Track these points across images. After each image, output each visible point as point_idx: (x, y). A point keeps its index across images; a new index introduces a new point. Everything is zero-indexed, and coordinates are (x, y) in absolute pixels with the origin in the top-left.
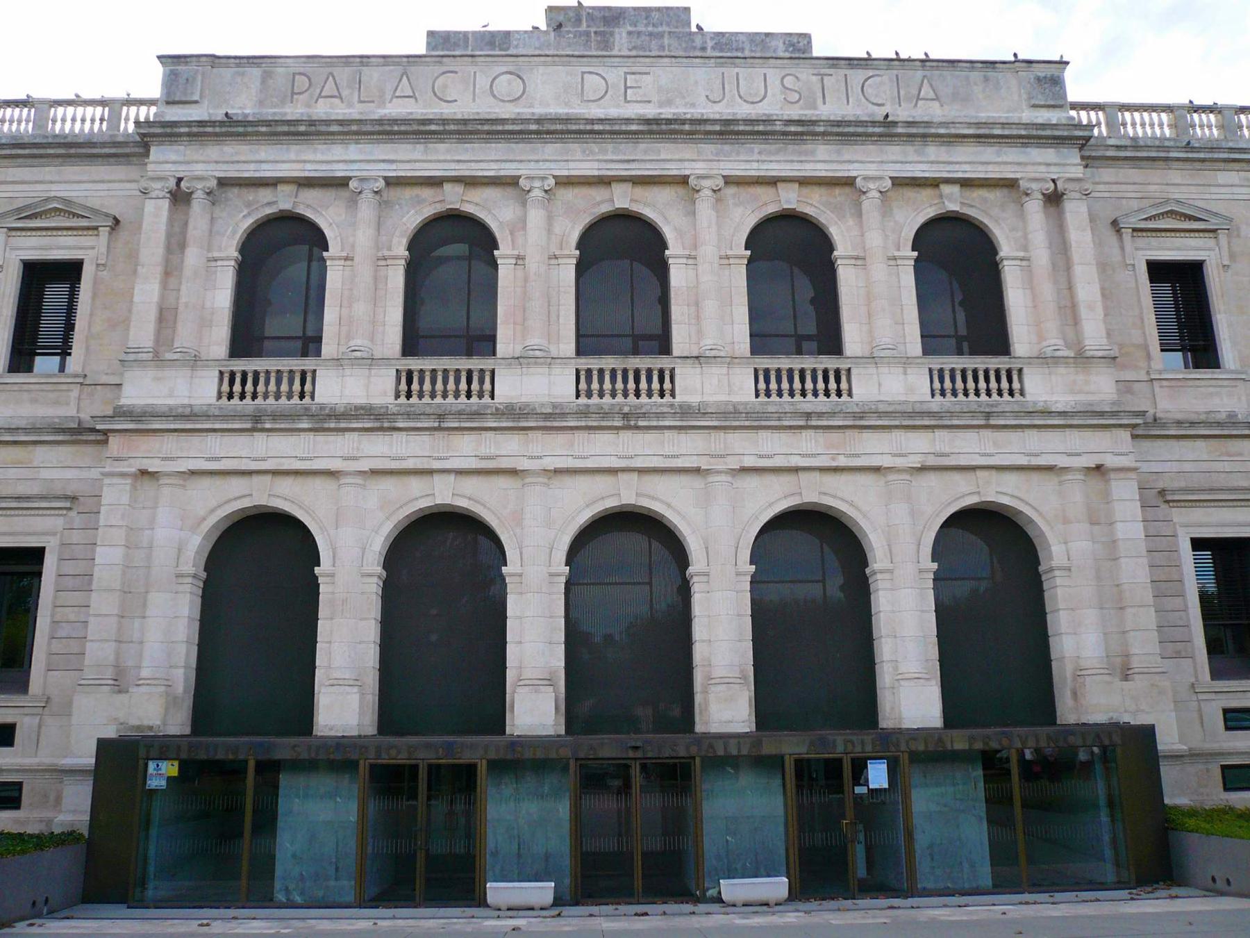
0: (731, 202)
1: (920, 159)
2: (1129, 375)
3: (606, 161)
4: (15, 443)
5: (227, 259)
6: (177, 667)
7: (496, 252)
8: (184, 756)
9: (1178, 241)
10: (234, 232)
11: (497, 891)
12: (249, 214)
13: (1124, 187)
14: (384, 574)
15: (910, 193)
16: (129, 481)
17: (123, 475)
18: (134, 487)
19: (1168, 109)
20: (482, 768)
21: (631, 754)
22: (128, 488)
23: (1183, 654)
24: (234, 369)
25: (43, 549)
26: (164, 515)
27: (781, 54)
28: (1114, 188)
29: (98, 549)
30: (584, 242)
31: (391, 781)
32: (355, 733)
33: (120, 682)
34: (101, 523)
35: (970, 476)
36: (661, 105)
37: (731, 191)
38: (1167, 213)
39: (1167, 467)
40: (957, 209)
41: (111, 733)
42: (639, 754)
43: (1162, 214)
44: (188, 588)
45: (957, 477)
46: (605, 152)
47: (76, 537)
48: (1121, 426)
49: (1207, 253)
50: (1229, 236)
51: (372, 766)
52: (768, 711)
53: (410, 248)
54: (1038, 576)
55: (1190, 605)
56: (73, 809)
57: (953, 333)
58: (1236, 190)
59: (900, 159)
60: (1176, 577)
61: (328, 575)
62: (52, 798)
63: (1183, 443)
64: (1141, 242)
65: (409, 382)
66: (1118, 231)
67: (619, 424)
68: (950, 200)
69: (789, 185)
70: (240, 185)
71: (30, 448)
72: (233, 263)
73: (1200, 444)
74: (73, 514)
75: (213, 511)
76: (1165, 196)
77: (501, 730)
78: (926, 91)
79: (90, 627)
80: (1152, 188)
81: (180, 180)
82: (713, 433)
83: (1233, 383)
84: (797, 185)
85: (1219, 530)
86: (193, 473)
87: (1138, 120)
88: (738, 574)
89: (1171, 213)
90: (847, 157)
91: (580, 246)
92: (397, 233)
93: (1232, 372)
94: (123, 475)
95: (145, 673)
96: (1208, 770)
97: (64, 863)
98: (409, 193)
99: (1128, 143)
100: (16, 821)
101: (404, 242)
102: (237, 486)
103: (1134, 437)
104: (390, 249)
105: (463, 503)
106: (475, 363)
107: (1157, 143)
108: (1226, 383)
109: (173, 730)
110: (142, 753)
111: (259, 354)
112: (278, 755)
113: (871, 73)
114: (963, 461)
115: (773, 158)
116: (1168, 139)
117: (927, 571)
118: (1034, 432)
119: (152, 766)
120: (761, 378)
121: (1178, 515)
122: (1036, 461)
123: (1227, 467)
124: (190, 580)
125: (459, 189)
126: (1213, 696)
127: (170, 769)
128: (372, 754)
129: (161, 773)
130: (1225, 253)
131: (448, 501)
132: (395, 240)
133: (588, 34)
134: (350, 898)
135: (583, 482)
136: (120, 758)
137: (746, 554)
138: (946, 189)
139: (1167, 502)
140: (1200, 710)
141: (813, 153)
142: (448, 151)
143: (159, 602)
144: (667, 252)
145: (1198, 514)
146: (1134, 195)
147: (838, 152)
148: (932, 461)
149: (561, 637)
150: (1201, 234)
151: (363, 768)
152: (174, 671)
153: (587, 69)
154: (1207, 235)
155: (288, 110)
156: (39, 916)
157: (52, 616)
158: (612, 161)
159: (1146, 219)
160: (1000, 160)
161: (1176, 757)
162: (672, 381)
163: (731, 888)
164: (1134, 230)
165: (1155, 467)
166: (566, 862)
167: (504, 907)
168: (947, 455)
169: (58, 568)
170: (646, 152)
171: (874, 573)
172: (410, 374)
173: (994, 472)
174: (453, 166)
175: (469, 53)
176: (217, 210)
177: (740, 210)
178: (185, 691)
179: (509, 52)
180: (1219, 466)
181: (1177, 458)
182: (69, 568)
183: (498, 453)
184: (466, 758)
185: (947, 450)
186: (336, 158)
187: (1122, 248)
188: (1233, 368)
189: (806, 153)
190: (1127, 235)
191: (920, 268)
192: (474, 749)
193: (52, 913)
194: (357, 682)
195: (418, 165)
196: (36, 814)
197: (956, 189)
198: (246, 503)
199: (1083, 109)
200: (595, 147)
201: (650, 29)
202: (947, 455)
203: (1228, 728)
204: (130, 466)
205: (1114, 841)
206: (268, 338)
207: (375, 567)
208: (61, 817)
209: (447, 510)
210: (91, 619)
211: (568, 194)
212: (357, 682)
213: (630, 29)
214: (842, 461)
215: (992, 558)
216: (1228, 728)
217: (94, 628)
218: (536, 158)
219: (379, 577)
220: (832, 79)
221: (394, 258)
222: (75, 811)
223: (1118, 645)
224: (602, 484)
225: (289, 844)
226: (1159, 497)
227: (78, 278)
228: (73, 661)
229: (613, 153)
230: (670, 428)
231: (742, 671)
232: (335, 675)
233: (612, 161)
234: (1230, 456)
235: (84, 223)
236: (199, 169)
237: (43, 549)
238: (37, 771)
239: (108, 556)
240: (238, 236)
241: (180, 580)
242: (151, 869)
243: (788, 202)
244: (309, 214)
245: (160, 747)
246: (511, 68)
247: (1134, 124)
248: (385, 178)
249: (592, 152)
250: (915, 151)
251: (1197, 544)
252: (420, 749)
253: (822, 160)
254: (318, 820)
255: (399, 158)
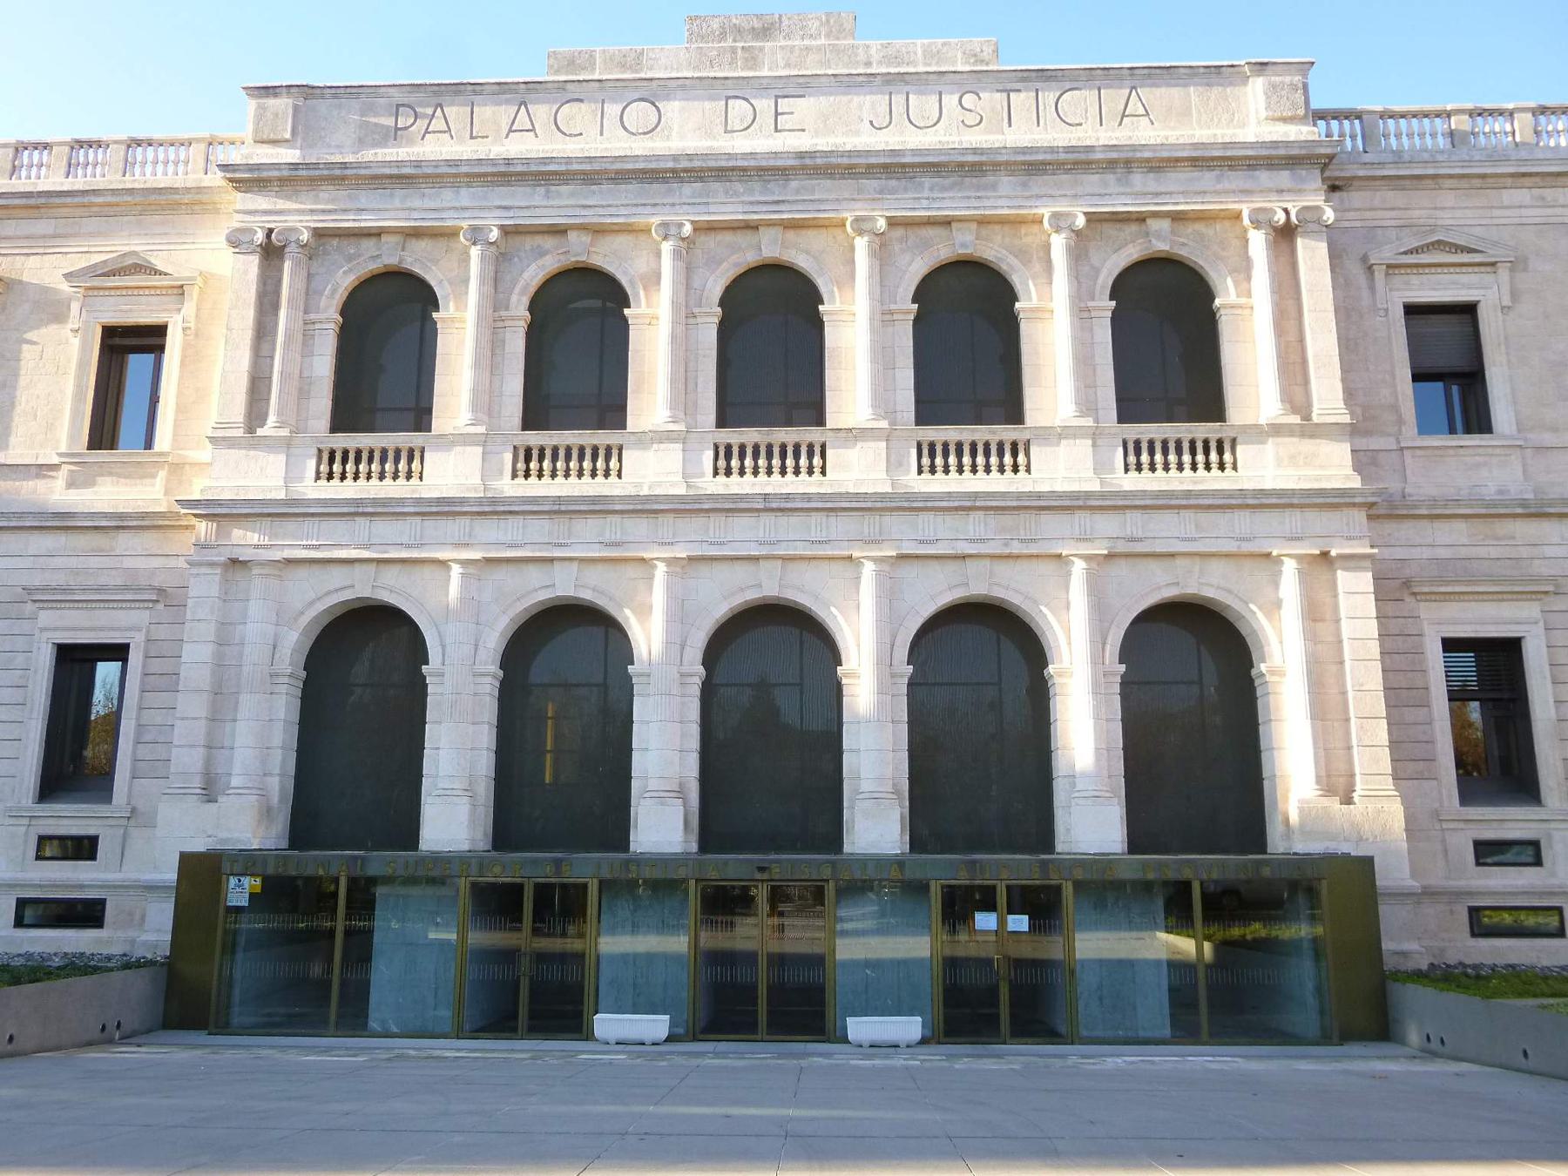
0: (897, 247)
1: (1122, 190)
2: (1376, 443)
3: (751, 203)
4: (96, 528)
5: (328, 321)
6: (271, 775)
7: (626, 311)
8: (270, 871)
9: (1444, 277)
10: (334, 291)
11: (607, 1024)
12: (350, 270)
13: (1380, 214)
14: (501, 673)
15: (1110, 229)
16: (218, 571)
17: (212, 564)
18: (225, 580)
19: (1359, 115)
20: (1068, 890)
21: (758, 876)
22: (217, 578)
23: (1426, 775)
24: (335, 446)
25: (127, 646)
26: (256, 608)
27: (960, 68)
28: (1368, 214)
29: (185, 646)
30: (729, 299)
31: (498, 903)
32: (466, 847)
33: (210, 790)
34: (189, 616)
35: (1167, 562)
36: (817, 133)
37: (899, 232)
38: (1433, 244)
39: (1415, 553)
40: (1167, 248)
41: (199, 845)
42: (765, 876)
43: (1428, 245)
44: (283, 689)
45: (1154, 566)
46: (751, 191)
47: (162, 632)
48: (1354, 505)
49: (1482, 292)
50: (1512, 270)
51: (474, 885)
52: (1143, 831)
53: (531, 309)
54: (1251, 681)
55: (1436, 715)
56: (148, 928)
57: (412, 404)
58: (1524, 212)
59: (1097, 191)
60: (1420, 684)
61: (641, 675)
62: (137, 917)
63: (1437, 524)
64: (1397, 280)
65: (528, 459)
66: (1370, 268)
67: (760, 506)
68: (1159, 237)
69: (966, 225)
70: (340, 236)
71: (113, 534)
72: (332, 326)
73: (1460, 525)
74: (160, 606)
75: (312, 603)
76: (1432, 222)
77: (623, 844)
78: (1135, 106)
79: (176, 731)
80: (1417, 213)
81: (271, 231)
82: (867, 515)
83: (1508, 451)
84: (974, 226)
85: (71, 634)
86: (289, 562)
87: (1405, 139)
88: (893, 676)
89: (1439, 245)
90: (1035, 190)
91: (722, 303)
92: (517, 290)
93: (1505, 437)
94: (212, 564)
95: (235, 782)
96: (1452, 912)
97: (139, 986)
98: (530, 242)
99: (1390, 158)
100: (98, 941)
101: (526, 301)
102: (337, 576)
103: (1369, 517)
104: (507, 308)
105: (587, 595)
106: (602, 438)
107: (1426, 156)
108: (1498, 451)
109: (270, 844)
110: (226, 867)
111: (371, 429)
112: (373, 870)
113: (1068, 85)
114: (1159, 547)
115: (945, 195)
116: (1442, 152)
117: (1113, 674)
118: (1247, 513)
119: (233, 881)
120: (925, 452)
121: (1426, 611)
122: (1247, 547)
123: (1494, 552)
124: (286, 680)
125: (586, 238)
126: (1462, 825)
127: (252, 884)
128: (474, 870)
129: (239, 890)
130: (1506, 289)
131: (571, 593)
132: (514, 298)
133: (733, 50)
134: (447, 1029)
135: (722, 572)
136: (201, 873)
137: (902, 652)
138: (1153, 224)
139: (1414, 594)
140: (1444, 841)
141: (994, 187)
142: (572, 195)
143: (249, 704)
144: (1017, 305)
145: (1452, 610)
146: (1393, 223)
147: (1024, 185)
148: (1121, 547)
149: (694, 743)
150: (1476, 269)
151: (463, 884)
152: (269, 779)
153: (731, 93)
154: (1483, 269)
155: (1219, 132)
156: (111, 1041)
157: (138, 719)
158: (759, 203)
159: (1405, 253)
160: (1219, 187)
161: (1402, 895)
162: (620, 460)
163: (860, 1028)
164: (1389, 266)
165: (1400, 553)
166: (685, 995)
167: (866, 1044)
168: (1140, 540)
169: (144, 666)
170: (798, 192)
171: (847, 675)
172: (528, 452)
173: (1197, 559)
174: (578, 212)
175: (596, 77)
176: (315, 266)
177: (908, 257)
178: (280, 801)
179: (643, 75)
180: (1482, 552)
181: (1429, 540)
182: (156, 666)
183: (625, 539)
184: (571, 876)
185: (1140, 535)
186: (445, 204)
187: (1372, 288)
188: (1507, 432)
189: (985, 188)
190: (1379, 275)
191: (1118, 322)
192: (586, 867)
193: (128, 1038)
194: (681, 793)
195: (538, 212)
196: (120, 934)
197: (1165, 224)
198: (348, 595)
199: (1334, 118)
200: (739, 187)
201: (807, 42)
202: (1140, 540)
203: (1478, 864)
204: (219, 555)
205: (1318, 989)
206: (383, 410)
207: (490, 666)
208: (144, 937)
209: (356, 606)
210: (178, 723)
211: (710, 241)
212: (681, 793)
213: (783, 43)
214: (1016, 548)
215: (1192, 664)
216: (1478, 864)
217: (180, 733)
218: (670, 201)
219: (494, 677)
220: (1023, 95)
221: (513, 318)
222: (159, 930)
223: (1336, 767)
224: (741, 572)
225: (384, 973)
226: (1395, 590)
227: (160, 349)
228: (156, 769)
229: (761, 193)
230: (817, 509)
231: (894, 785)
232: (441, 785)
233: (759, 203)
234: (1498, 539)
235: (1477, 258)
236: (292, 221)
237: (127, 646)
238: (115, 887)
239: (196, 656)
240: (337, 296)
241: (479, 680)
242: (237, 992)
243: (963, 245)
244: (417, 270)
245: (247, 861)
246: (645, 94)
247: (1398, 136)
248: (502, 227)
249: (736, 194)
250: (1119, 180)
251: (1450, 645)
252: (528, 868)
253: (1179, 193)
254: (422, 944)
255: (517, 204)
